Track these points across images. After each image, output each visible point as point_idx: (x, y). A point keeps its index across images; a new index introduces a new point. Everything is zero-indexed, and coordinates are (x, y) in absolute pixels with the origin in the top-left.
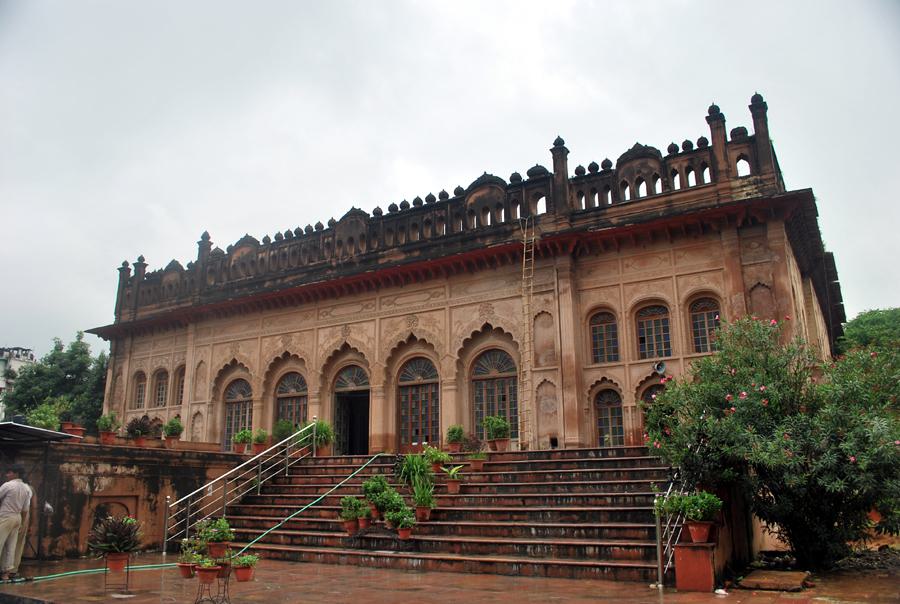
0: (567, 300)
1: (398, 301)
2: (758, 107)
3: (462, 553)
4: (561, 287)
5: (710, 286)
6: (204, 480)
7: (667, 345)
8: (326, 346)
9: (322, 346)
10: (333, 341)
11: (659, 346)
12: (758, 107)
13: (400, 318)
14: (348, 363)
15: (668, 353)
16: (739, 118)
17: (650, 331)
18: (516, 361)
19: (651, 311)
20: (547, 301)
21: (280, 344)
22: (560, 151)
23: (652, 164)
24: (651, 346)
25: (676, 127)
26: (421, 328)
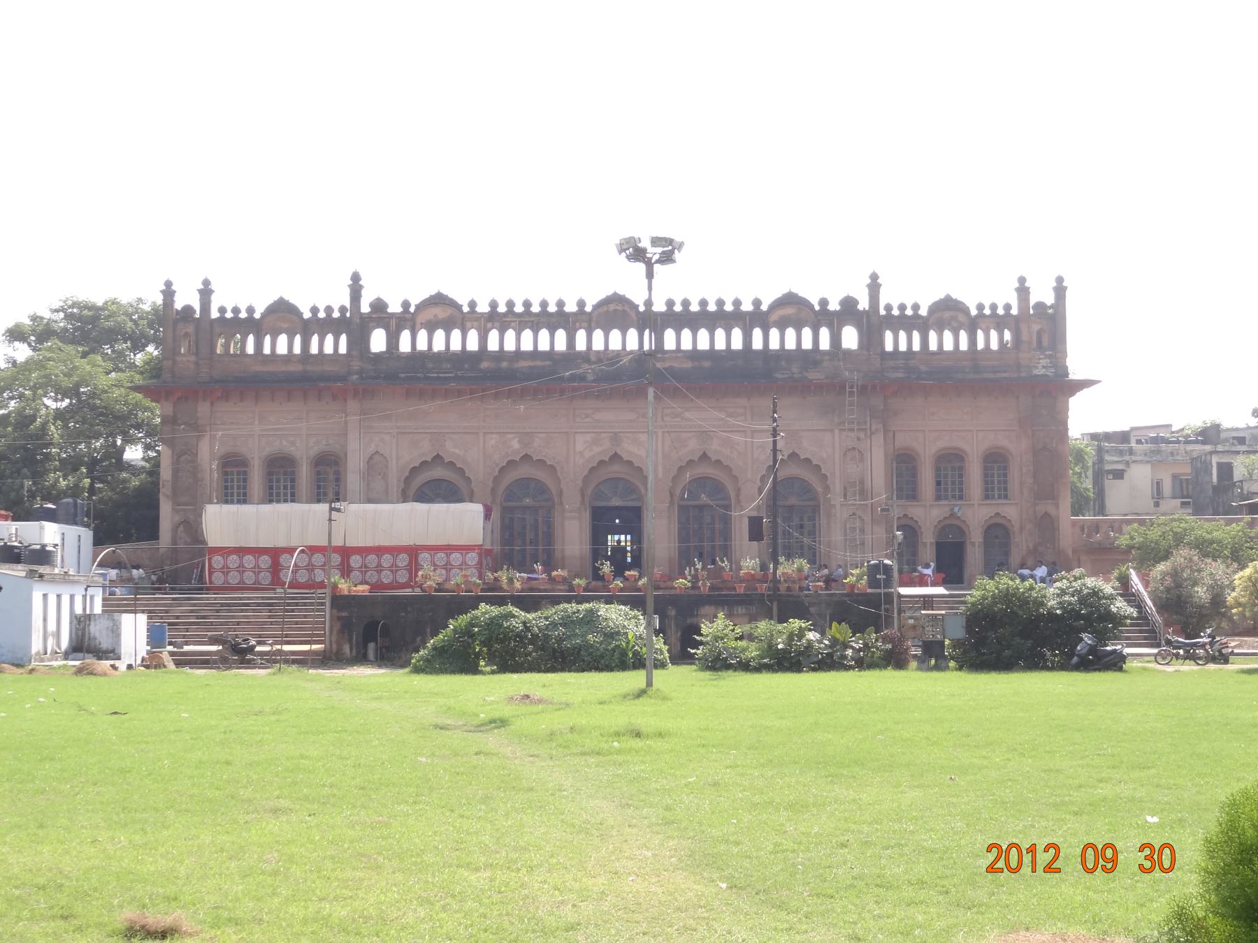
0: (879, 439)
1: (687, 415)
2: (1060, 290)
3: (280, 652)
4: (873, 428)
5: (1005, 443)
6: (665, 643)
7: (961, 490)
8: (587, 454)
9: (581, 453)
10: (597, 450)
11: (953, 490)
12: (1060, 290)
13: (690, 435)
14: (612, 476)
15: (961, 498)
16: (1042, 294)
17: (946, 476)
18: (732, 495)
19: (950, 463)
20: (859, 439)
21: (515, 444)
22: (874, 287)
23: (961, 318)
24: (946, 490)
25: (986, 290)
26: (452, 450)
